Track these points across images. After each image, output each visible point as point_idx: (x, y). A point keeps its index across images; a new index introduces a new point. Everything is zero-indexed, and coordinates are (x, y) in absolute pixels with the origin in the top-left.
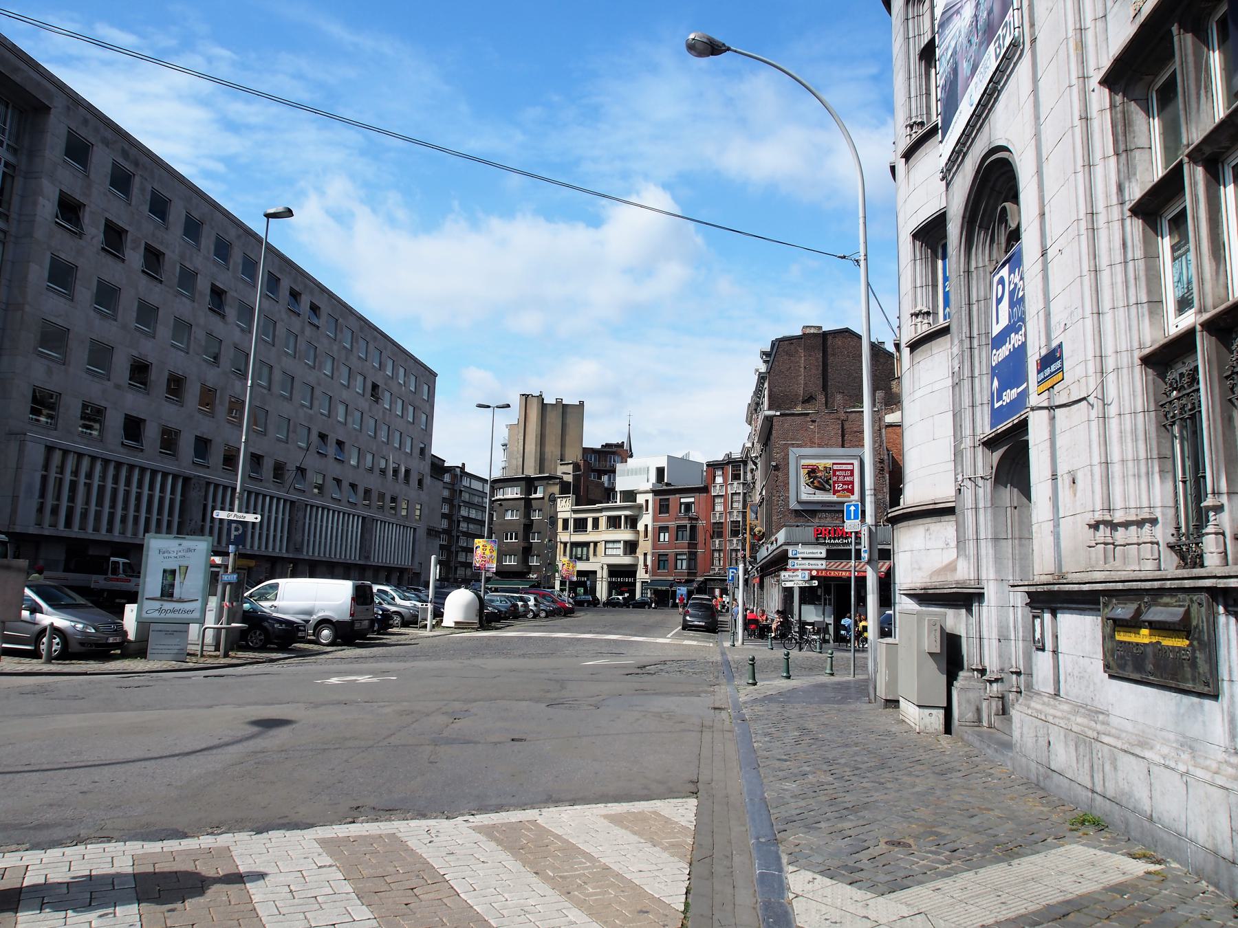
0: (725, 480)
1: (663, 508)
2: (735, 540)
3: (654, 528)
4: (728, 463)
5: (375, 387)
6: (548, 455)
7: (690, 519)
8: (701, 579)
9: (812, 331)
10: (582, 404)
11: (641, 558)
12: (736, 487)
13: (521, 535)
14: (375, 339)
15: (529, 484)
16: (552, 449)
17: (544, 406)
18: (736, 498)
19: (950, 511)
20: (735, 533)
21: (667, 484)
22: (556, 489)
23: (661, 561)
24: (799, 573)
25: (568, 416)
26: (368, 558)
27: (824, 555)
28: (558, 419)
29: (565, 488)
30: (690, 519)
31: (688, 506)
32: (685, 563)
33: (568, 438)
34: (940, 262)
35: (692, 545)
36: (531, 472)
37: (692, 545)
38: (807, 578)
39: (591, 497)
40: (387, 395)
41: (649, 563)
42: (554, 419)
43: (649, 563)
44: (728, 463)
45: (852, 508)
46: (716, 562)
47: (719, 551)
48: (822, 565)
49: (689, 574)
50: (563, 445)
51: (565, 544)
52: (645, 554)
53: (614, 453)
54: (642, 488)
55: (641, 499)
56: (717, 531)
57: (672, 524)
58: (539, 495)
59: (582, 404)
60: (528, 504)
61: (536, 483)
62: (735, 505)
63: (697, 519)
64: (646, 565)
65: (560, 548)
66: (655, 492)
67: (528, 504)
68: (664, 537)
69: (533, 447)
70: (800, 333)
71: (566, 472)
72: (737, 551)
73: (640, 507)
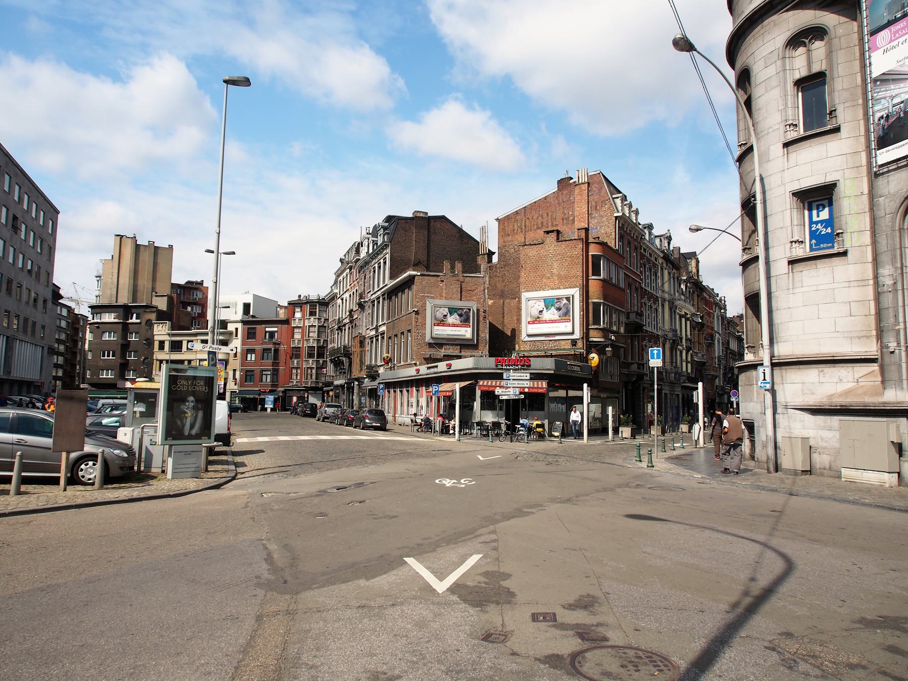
0: (303, 316)
1: (250, 334)
2: (311, 361)
3: (242, 350)
4: (306, 303)
5: (15, 218)
6: (140, 288)
7: (274, 344)
8: (283, 389)
9: (421, 215)
10: (171, 247)
11: (231, 373)
12: (313, 321)
13: (118, 353)
14: (16, 175)
15: (126, 311)
16: (144, 282)
17: (137, 247)
18: (312, 329)
19: (873, 361)
20: (310, 355)
21: (253, 316)
22: (153, 316)
23: (248, 376)
24: (511, 390)
25: (159, 256)
26: (9, 373)
27: (528, 378)
28: (149, 258)
29: (162, 316)
30: (274, 344)
31: (272, 334)
32: (269, 377)
33: (158, 275)
34: (806, 212)
35: (276, 363)
36: (124, 299)
37: (276, 363)
38: (518, 393)
39: (182, 324)
40: (23, 226)
41: (238, 376)
42: (146, 258)
43: (238, 376)
44: (306, 303)
45: (655, 352)
46: (294, 377)
47: (297, 368)
48: (527, 384)
49: (272, 386)
50: (154, 280)
51: (161, 361)
52: (235, 370)
53: (196, 289)
54: (232, 319)
55: (231, 327)
56: (296, 353)
57: (258, 347)
58: (134, 320)
59: (171, 247)
60: (125, 328)
61: (133, 310)
62: (311, 334)
63: (279, 344)
64: (234, 378)
65: (156, 365)
66: (244, 322)
67: (125, 328)
68: (251, 357)
69: (127, 280)
70: (411, 216)
71: (161, 304)
72: (312, 368)
73: (231, 333)
